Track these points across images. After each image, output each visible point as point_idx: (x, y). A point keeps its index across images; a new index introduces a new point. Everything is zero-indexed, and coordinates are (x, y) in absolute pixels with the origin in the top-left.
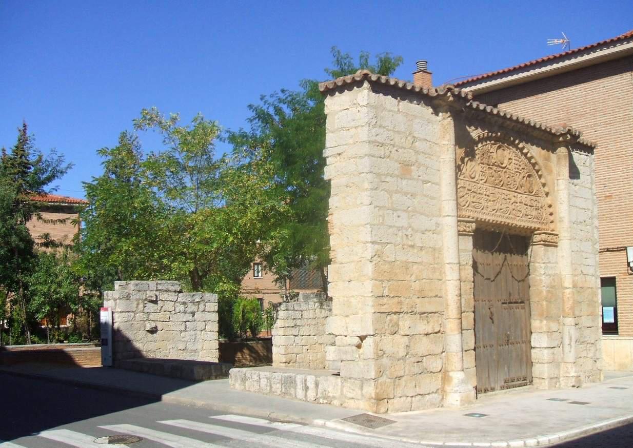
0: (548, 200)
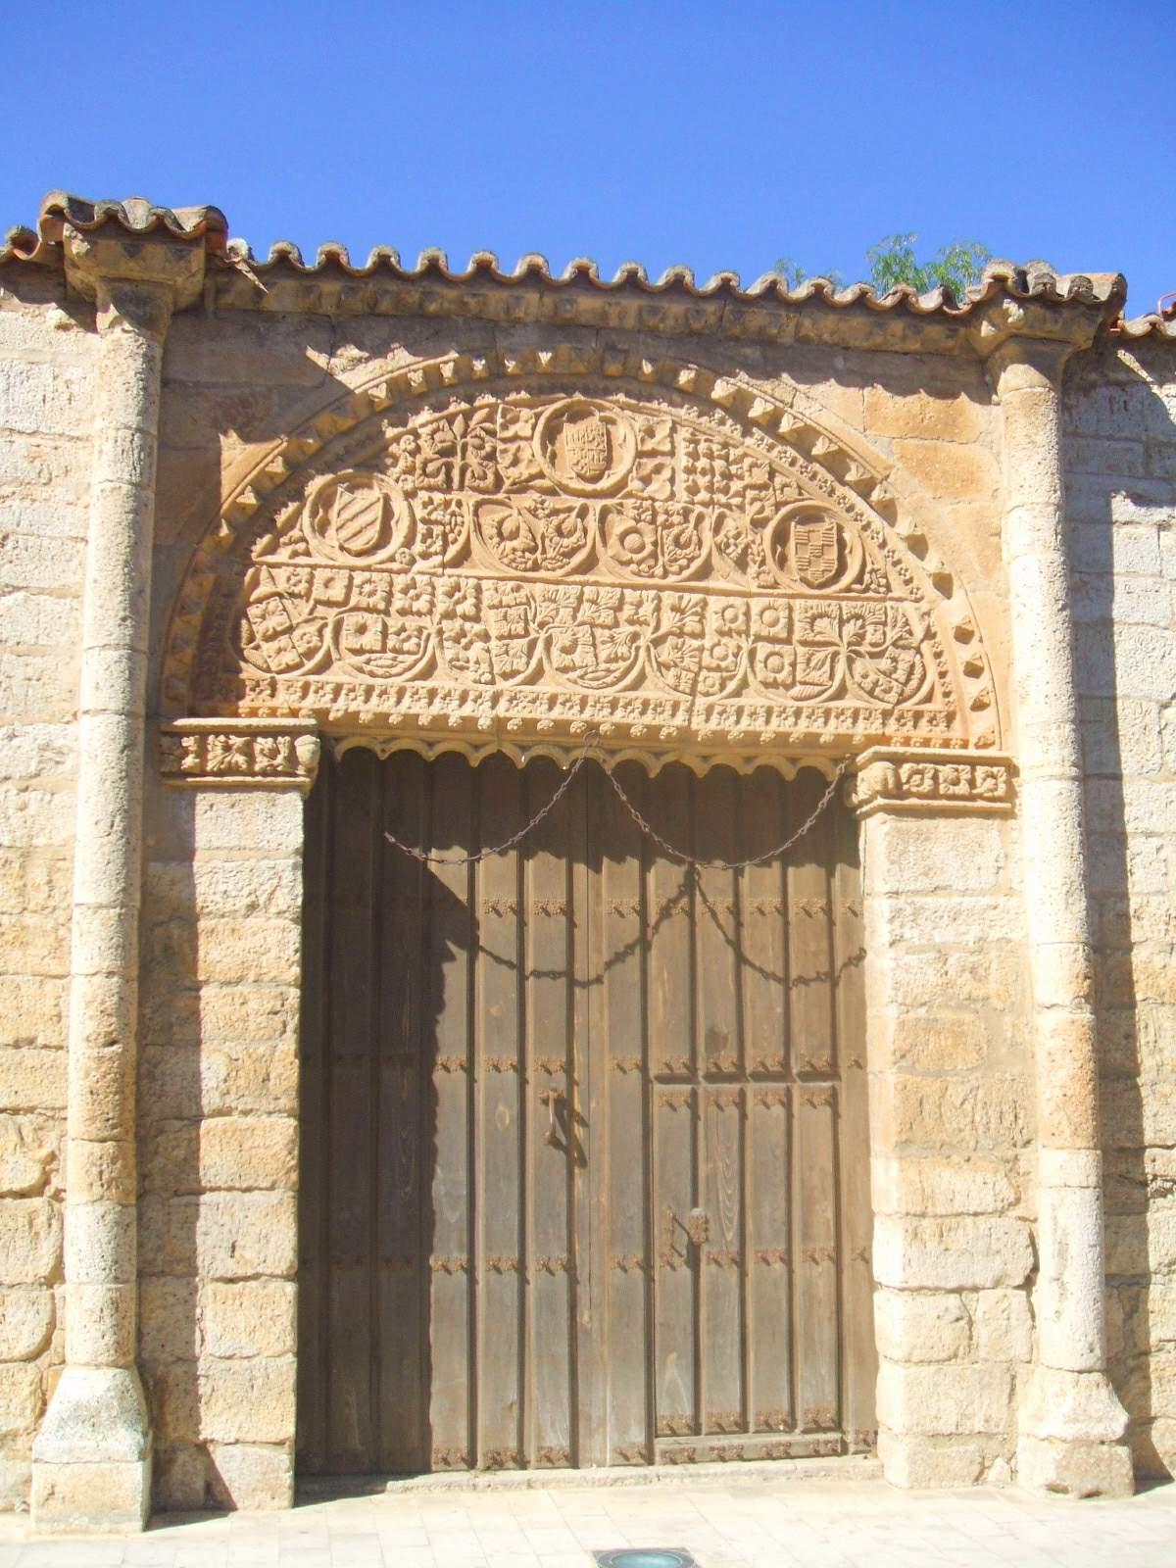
0: (952, 612)
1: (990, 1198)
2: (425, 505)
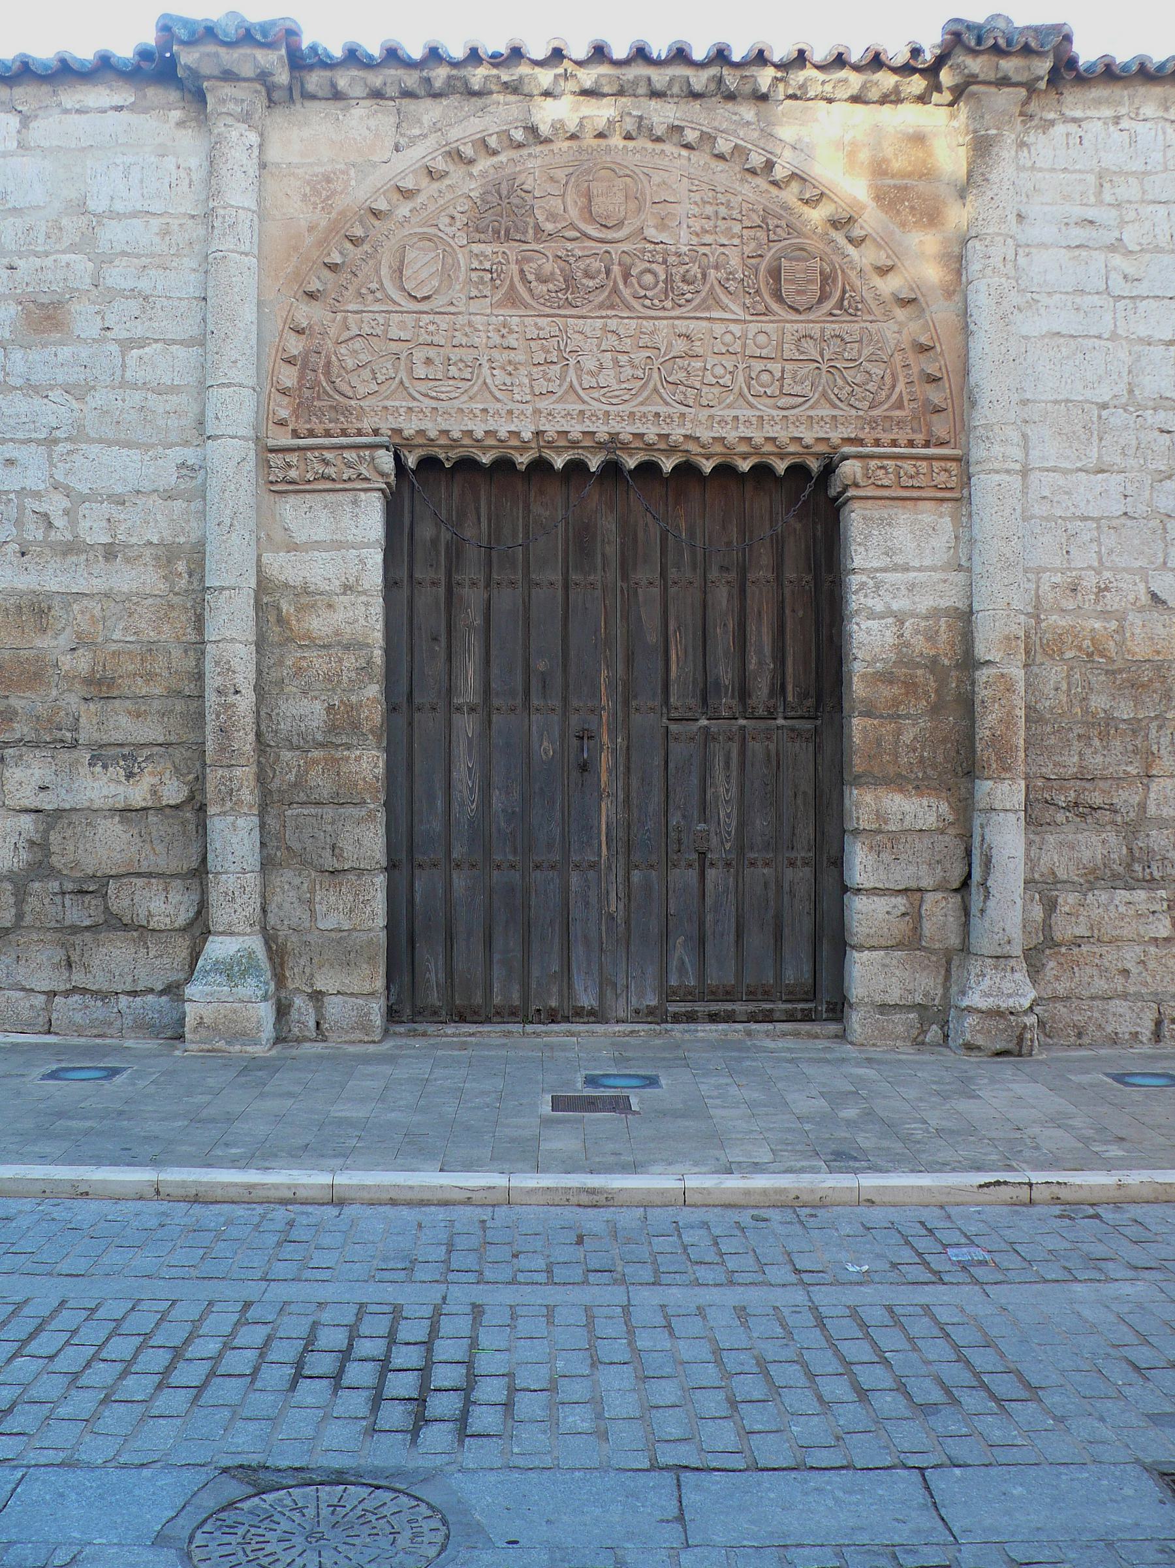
1: (933, 819)
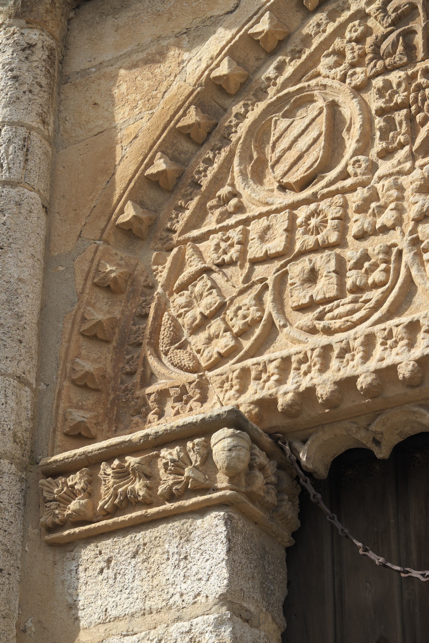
2: (381, 93)
